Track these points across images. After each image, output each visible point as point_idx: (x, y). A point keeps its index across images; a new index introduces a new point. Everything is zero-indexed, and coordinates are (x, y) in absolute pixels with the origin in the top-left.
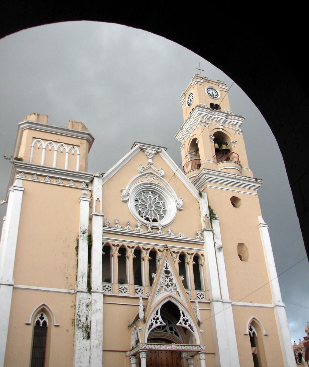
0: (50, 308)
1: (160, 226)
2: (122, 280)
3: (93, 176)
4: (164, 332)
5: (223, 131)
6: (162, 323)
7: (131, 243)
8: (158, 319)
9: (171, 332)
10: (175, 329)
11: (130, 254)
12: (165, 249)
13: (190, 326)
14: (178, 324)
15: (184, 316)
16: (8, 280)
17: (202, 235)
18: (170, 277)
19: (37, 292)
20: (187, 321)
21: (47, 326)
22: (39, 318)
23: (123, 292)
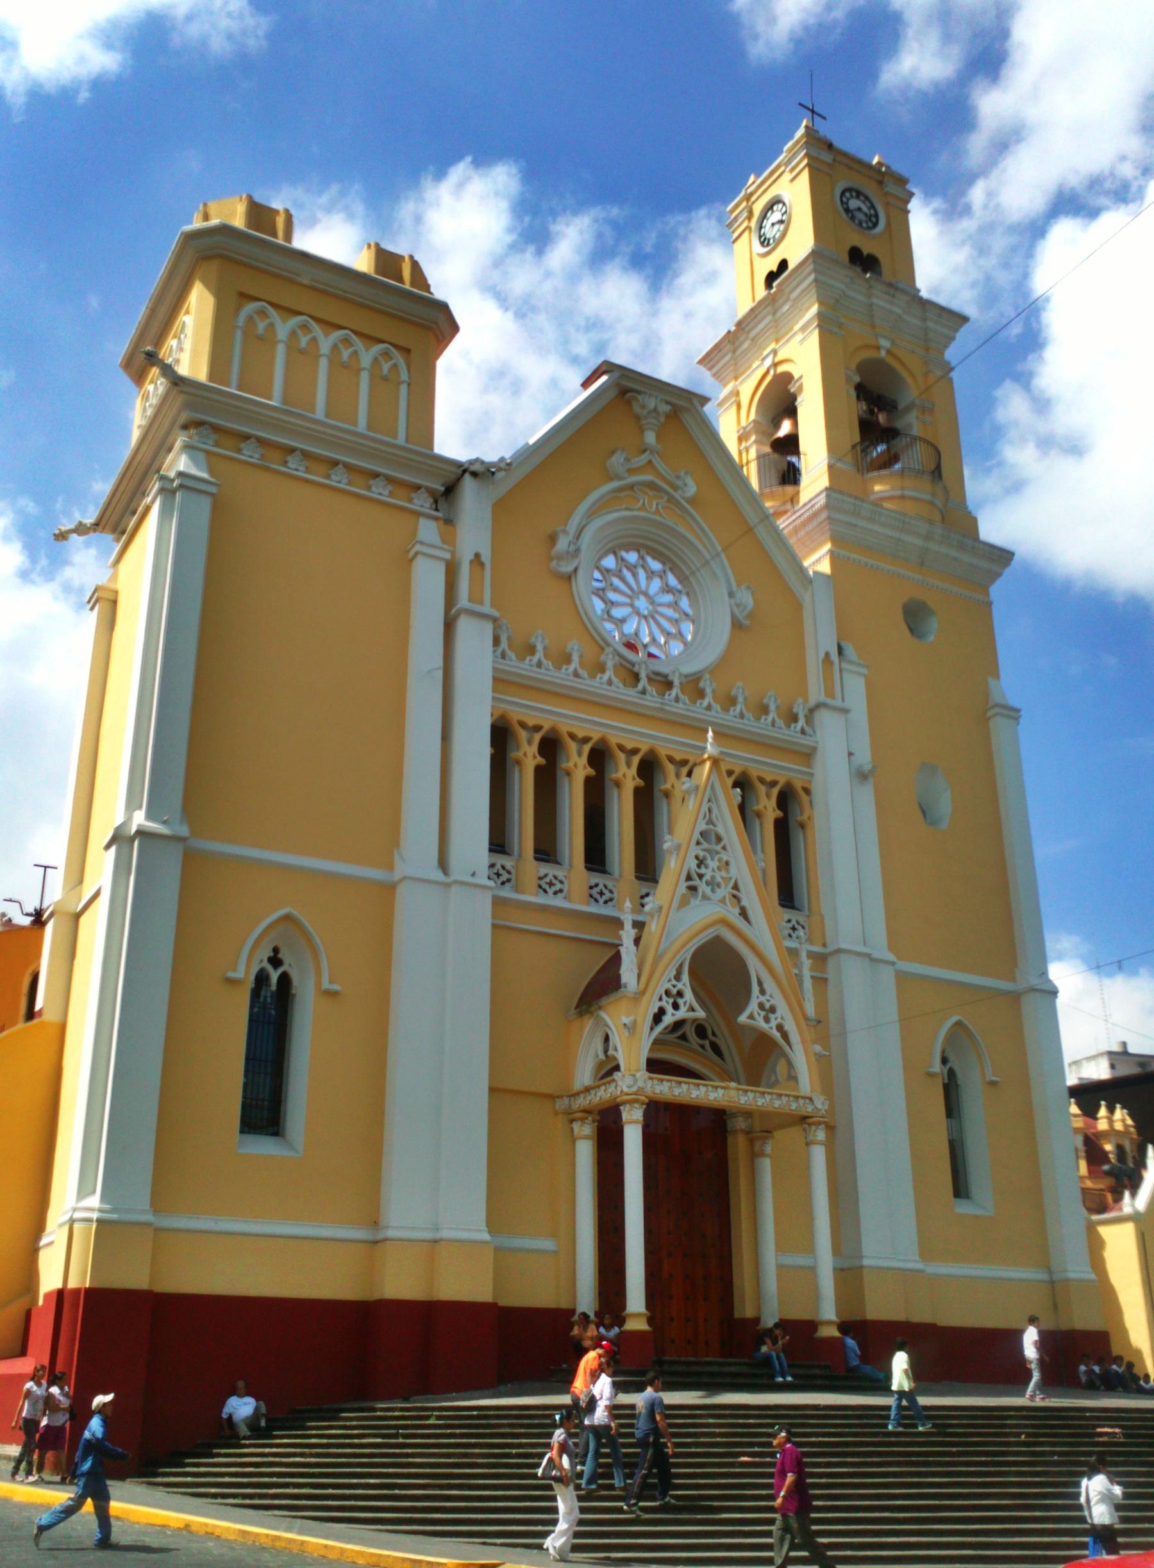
0: (310, 929)
1: (677, 675)
2: (546, 851)
8: (680, 994)
9: (701, 1042)
11: (577, 766)
13: (780, 1028)
14: (743, 1018)
15: (763, 992)
17: (809, 720)
20: (773, 1010)
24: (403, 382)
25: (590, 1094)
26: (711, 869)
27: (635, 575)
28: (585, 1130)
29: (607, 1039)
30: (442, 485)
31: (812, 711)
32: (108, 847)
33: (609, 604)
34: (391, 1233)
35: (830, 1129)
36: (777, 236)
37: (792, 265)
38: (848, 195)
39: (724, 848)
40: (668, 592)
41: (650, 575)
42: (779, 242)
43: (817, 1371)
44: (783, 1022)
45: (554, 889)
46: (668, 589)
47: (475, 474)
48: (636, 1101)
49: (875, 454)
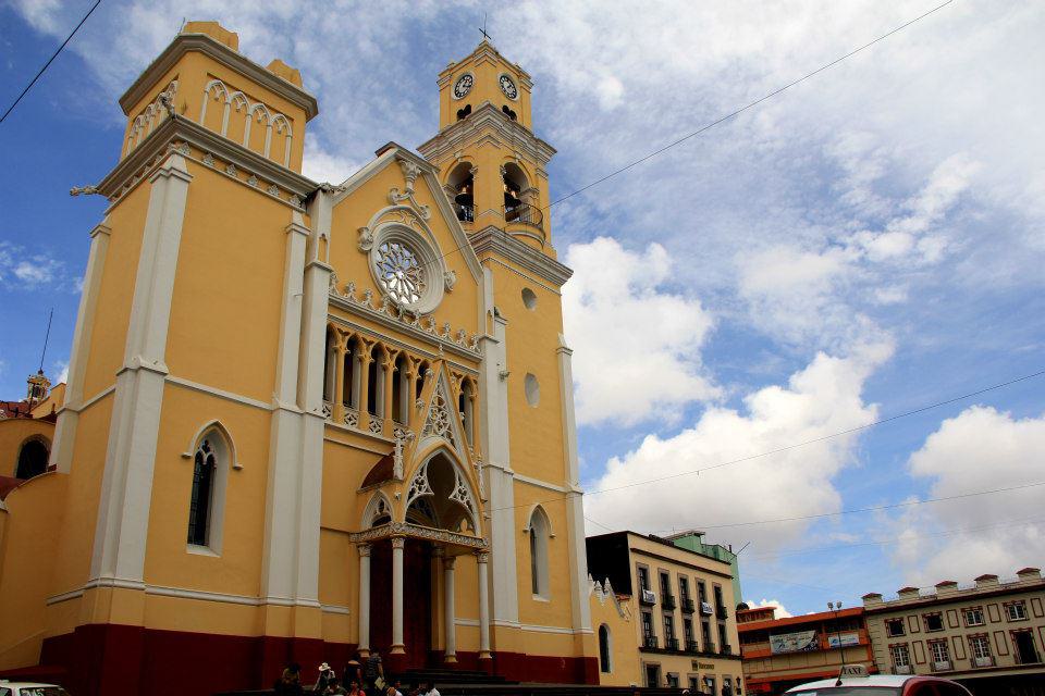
5: (519, 165)
7: (368, 332)
8: (423, 481)
13: (468, 503)
14: (451, 497)
17: (479, 346)
19: (187, 393)
20: (465, 493)
29: (382, 504)
31: (481, 340)
34: (269, 601)
37: (473, 110)
47: (324, 191)
48: (400, 537)
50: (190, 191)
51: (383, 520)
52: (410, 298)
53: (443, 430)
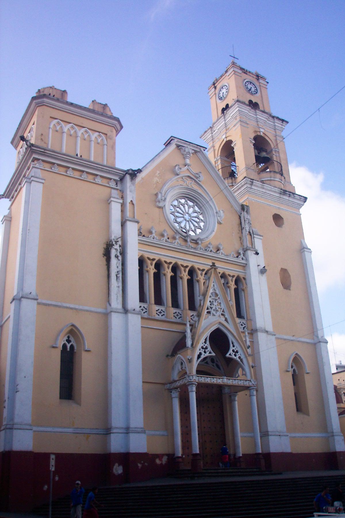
2: (159, 301)
3: (124, 173)
4: (205, 364)
6: (211, 353)
10: (217, 361)
12: (212, 268)
13: (239, 357)
14: (228, 355)
15: (234, 346)
16: (31, 293)
18: (218, 301)
20: (237, 352)
21: (75, 351)
22: (65, 340)
23: (160, 315)
24: (105, 145)
25: (177, 383)
26: (215, 305)
27: (184, 207)
28: (175, 395)
30: (119, 178)
32: (11, 303)
33: (176, 217)
34: (15, 426)
35: (257, 391)
36: (226, 94)
38: (247, 83)
39: (219, 298)
40: (195, 212)
41: (189, 207)
42: (225, 98)
43: (270, 500)
44: (241, 356)
45: (162, 314)
46: (195, 212)
49: (260, 167)
50: (44, 187)
51: (183, 374)
52: (194, 231)
53: (219, 313)
